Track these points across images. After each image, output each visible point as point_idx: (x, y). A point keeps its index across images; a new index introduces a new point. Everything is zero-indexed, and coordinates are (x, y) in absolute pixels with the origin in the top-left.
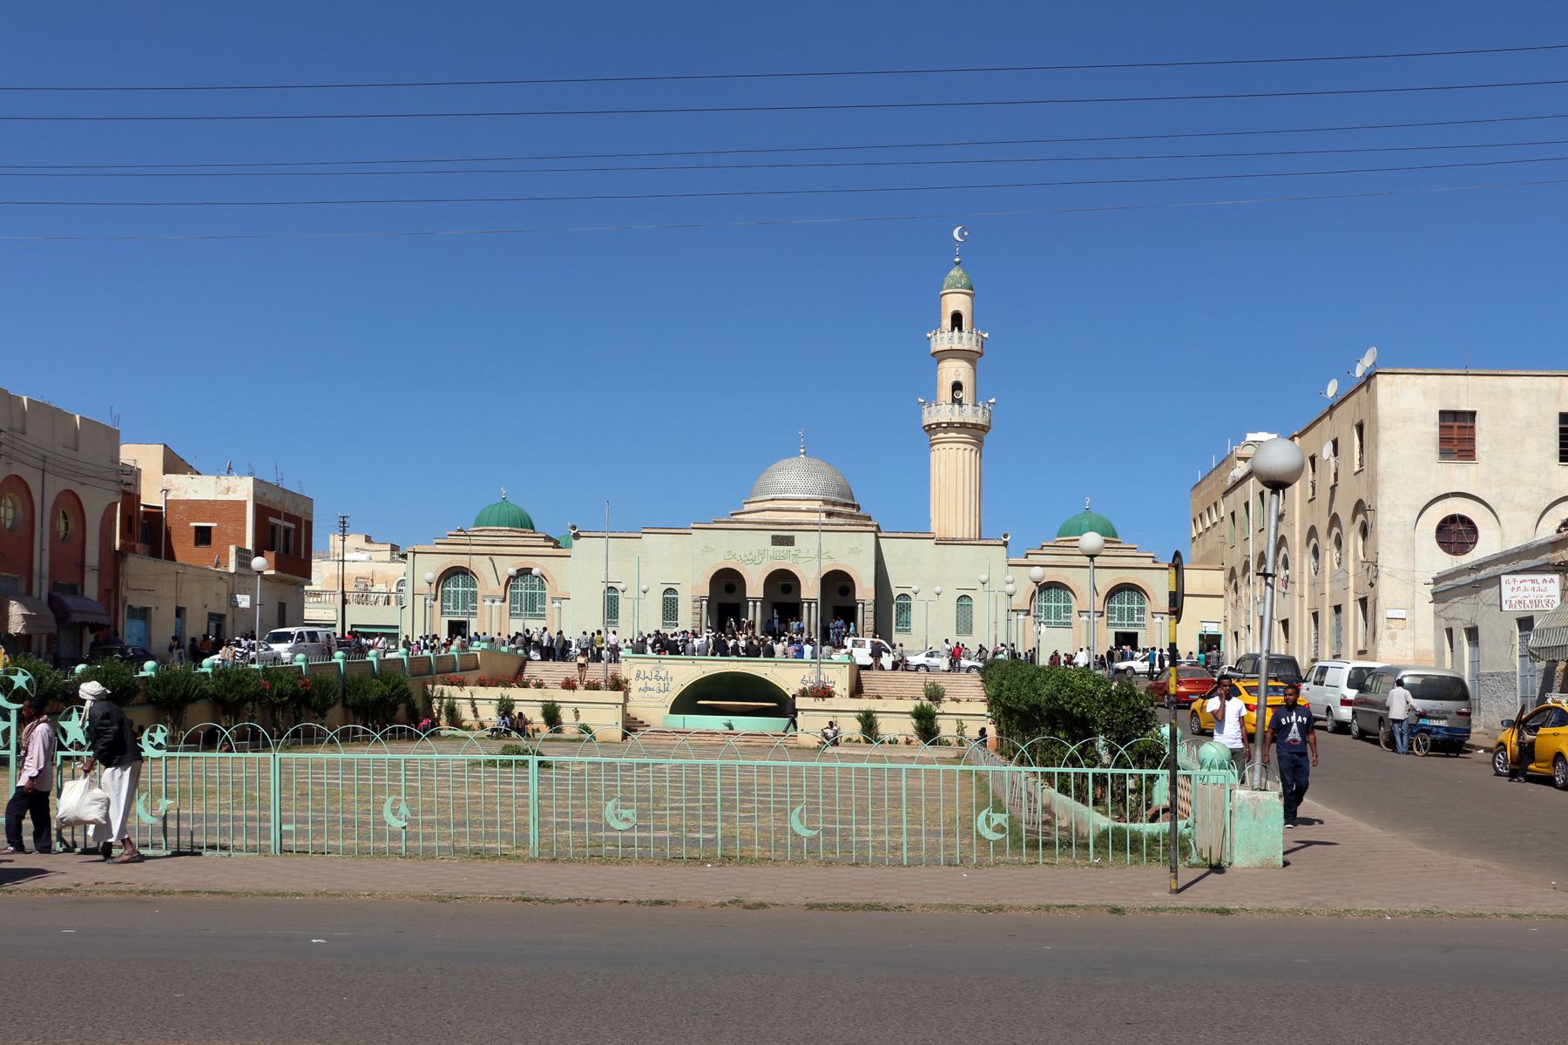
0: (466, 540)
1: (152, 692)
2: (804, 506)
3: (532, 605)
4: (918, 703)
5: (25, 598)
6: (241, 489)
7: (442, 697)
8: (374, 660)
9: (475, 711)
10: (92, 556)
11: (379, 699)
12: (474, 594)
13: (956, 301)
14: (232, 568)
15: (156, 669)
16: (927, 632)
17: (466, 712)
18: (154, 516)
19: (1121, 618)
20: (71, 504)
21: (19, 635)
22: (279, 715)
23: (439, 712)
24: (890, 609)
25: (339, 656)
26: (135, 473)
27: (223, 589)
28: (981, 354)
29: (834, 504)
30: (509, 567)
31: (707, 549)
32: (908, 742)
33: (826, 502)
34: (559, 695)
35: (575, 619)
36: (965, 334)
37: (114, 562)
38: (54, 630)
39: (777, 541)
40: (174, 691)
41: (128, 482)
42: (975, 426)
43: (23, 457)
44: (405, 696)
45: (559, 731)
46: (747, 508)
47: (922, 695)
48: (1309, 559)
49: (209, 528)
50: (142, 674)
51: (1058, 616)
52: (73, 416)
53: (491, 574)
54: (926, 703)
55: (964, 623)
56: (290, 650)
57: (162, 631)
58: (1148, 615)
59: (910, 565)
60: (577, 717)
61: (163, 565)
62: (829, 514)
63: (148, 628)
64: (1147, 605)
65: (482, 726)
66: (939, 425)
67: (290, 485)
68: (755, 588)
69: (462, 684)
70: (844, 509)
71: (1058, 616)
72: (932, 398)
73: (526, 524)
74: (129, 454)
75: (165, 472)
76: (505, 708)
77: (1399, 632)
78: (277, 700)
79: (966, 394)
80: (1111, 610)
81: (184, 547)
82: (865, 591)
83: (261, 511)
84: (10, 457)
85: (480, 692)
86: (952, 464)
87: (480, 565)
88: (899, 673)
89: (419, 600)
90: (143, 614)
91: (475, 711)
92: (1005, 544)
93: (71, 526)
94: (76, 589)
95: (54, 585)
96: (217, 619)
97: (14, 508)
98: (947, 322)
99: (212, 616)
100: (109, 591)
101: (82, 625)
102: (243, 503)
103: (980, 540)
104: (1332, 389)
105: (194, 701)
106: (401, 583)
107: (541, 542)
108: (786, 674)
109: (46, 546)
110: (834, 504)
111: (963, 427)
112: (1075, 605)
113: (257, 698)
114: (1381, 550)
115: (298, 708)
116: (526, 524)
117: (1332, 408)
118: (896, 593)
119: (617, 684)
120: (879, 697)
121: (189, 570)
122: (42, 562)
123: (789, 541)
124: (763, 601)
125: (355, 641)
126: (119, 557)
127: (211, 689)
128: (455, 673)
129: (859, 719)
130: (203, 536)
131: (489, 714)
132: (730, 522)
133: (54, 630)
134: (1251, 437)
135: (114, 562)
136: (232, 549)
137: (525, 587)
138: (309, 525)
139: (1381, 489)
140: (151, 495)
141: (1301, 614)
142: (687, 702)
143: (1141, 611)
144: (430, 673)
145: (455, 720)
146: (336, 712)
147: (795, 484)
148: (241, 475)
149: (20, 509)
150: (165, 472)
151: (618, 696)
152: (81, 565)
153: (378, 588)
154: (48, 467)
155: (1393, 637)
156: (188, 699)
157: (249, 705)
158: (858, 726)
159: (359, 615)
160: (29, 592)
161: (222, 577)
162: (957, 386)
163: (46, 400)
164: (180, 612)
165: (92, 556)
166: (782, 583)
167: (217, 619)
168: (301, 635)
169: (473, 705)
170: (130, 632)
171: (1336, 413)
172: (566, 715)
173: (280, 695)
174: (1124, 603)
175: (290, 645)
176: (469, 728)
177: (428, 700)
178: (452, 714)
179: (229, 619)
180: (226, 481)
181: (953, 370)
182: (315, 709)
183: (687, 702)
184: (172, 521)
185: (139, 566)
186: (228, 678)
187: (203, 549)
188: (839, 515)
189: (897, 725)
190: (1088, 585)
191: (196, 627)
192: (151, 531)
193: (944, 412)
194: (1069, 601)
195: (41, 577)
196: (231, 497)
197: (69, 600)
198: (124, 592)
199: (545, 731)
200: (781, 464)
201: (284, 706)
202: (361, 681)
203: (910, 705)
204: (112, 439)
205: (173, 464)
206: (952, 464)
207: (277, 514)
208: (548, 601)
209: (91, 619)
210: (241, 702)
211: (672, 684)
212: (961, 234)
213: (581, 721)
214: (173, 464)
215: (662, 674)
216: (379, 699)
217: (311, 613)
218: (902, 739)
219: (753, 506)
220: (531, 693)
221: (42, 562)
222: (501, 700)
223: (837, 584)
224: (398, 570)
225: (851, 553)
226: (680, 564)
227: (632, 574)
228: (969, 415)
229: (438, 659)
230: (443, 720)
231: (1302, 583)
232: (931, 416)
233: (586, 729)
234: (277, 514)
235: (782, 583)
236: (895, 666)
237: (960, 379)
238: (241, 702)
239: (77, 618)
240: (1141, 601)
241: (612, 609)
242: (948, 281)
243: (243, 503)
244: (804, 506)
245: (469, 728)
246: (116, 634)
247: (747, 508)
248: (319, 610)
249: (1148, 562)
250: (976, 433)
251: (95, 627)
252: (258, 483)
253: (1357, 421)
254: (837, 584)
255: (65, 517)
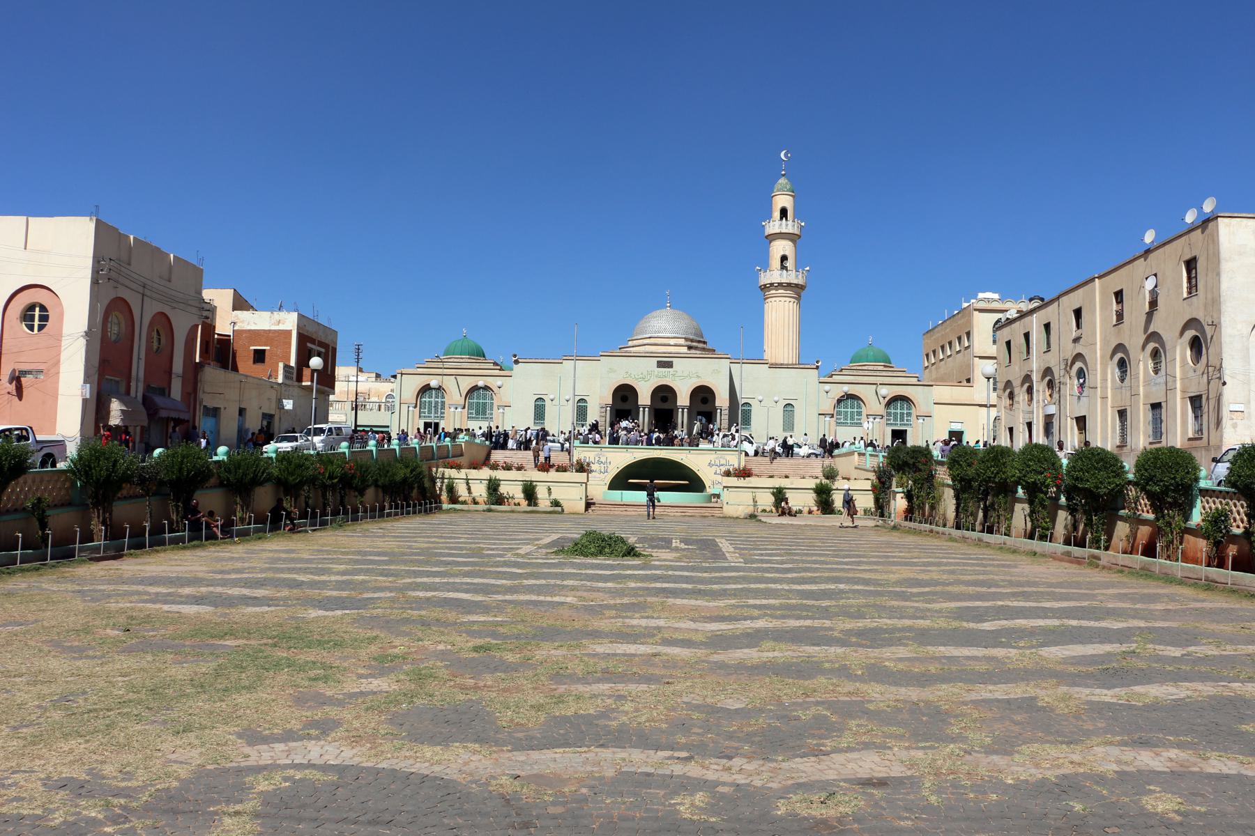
0: (440, 365)
1: (224, 475)
2: (672, 342)
3: (482, 412)
4: (818, 481)
5: (124, 397)
6: (288, 322)
7: (443, 478)
8: (397, 448)
9: (469, 489)
10: (178, 366)
11: (396, 483)
12: (443, 403)
13: (783, 200)
14: (280, 380)
15: (228, 454)
16: (765, 427)
17: (461, 490)
18: (225, 342)
19: (895, 419)
20: (163, 323)
21: (117, 426)
22: (329, 495)
23: (441, 489)
24: (739, 414)
25: (372, 445)
26: (212, 310)
27: (273, 395)
28: (799, 237)
29: (692, 341)
30: (467, 383)
31: (612, 370)
32: (810, 512)
33: (686, 339)
34: (534, 475)
35: (514, 417)
36: (790, 223)
37: (194, 372)
38: (145, 424)
39: (661, 365)
40: (245, 474)
41: (207, 313)
42: (797, 285)
43: (127, 283)
44: (419, 477)
45: (536, 505)
46: (630, 343)
47: (820, 475)
48: (1113, 371)
49: (264, 351)
50: (215, 458)
51: (852, 418)
52: (168, 255)
53: (455, 390)
54: (825, 481)
55: (789, 424)
56: (322, 441)
57: (229, 425)
58: (914, 417)
59: (756, 385)
60: (550, 493)
61: (231, 375)
62: (690, 348)
63: (218, 424)
64: (913, 411)
65: (475, 503)
66: (772, 284)
67: (323, 321)
68: (644, 399)
69: (459, 467)
70: (698, 345)
71: (852, 418)
72: (766, 266)
73: (481, 354)
74: (207, 294)
75: (234, 309)
76: (493, 486)
77: (1239, 422)
78: (329, 482)
79: (790, 264)
80: (889, 414)
81: (245, 364)
82: (722, 400)
83: (302, 338)
84: (117, 282)
85: (473, 473)
86: (780, 314)
87: (449, 383)
88: (759, 458)
89: (404, 407)
90: (214, 412)
91: (469, 489)
92: (817, 368)
93: (163, 341)
94: (164, 391)
95: (148, 388)
96: (268, 417)
97: (119, 324)
98: (777, 214)
99: (265, 416)
100: (189, 394)
101: (168, 419)
102: (289, 332)
103: (799, 365)
104: (1149, 237)
105: (261, 484)
106: (389, 396)
107: (491, 366)
108: (698, 460)
109: (143, 355)
110: (692, 341)
111: (789, 286)
112: (864, 411)
113: (312, 481)
114: (1225, 356)
115: (343, 488)
116: (481, 354)
117: (1148, 252)
118: (742, 401)
119: (582, 468)
120: (787, 477)
121: (250, 380)
122: (138, 368)
123: (669, 365)
124: (650, 407)
125: (358, 435)
126: (198, 367)
127: (275, 472)
128: (452, 458)
129: (773, 494)
130: (259, 356)
131: (480, 491)
132: (622, 352)
133: (145, 424)
134: (981, 295)
135: (194, 372)
136: (281, 365)
137: (478, 397)
138: (334, 350)
139: (1223, 308)
140: (223, 327)
141: (1104, 411)
142: (621, 481)
143: (909, 414)
144: (433, 459)
145: (454, 499)
146: (370, 493)
147: (665, 326)
148: (288, 311)
149: (123, 325)
150: (234, 309)
151: (582, 477)
152: (169, 372)
153: (372, 399)
154: (148, 293)
155: (1235, 426)
156: (256, 482)
157: (306, 488)
158: (773, 499)
159: (365, 419)
160: (128, 392)
161: (273, 386)
162: (784, 258)
163: (148, 240)
164: (242, 412)
165: (178, 366)
166: (664, 394)
167: (268, 417)
168: (330, 429)
169: (468, 484)
170: (204, 424)
171: (1152, 256)
172: (541, 492)
173: (331, 477)
174: (898, 409)
175: (322, 437)
176: (464, 503)
177: (433, 480)
178: (451, 490)
179: (277, 418)
180: (278, 315)
181: (781, 247)
182: (356, 489)
183: (621, 481)
184: (237, 346)
185: (213, 374)
186: (290, 462)
187: (259, 366)
188: (696, 348)
189: (803, 499)
190: (873, 398)
191: (254, 424)
192: (222, 352)
193: (775, 275)
194: (859, 407)
195: (137, 380)
196: (281, 327)
197: (158, 400)
198: (201, 395)
199: (524, 503)
200: (654, 314)
201: (333, 486)
202: (389, 465)
203: (812, 483)
204: (196, 277)
205: (240, 304)
206: (780, 314)
207: (313, 341)
208: (495, 408)
209: (174, 415)
210: (300, 485)
211: (610, 467)
212: (786, 155)
213: (553, 497)
214: (240, 304)
215: (603, 459)
216: (396, 483)
217: (332, 417)
218: (806, 510)
219: (635, 343)
220: (513, 474)
221: (138, 368)
222: (490, 480)
223: (703, 396)
224: (385, 387)
225: (713, 374)
226: (595, 382)
227: (553, 388)
228: (792, 277)
229: (438, 447)
230: (444, 497)
231: (1104, 388)
232: (765, 279)
233: (556, 503)
234: (313, 341)
235: (664, 394)
236: (756, 453)
237: (787, 253)
238: (300, 485)
239: (163, 414)
240: (909, 408)
241: (540, 412)
242: (777, 186)
243: (289, 332)
244: (672, 342)
245: (464, 503)
246: (194, 427)
247: (630, 343)
248: (339, 415)
249: (914, 381)
250: (797, 290)
251: (178, 422)
252: (301, 317)
253: (1188, 257)
254: (703, 396)
255: (158, 334)
